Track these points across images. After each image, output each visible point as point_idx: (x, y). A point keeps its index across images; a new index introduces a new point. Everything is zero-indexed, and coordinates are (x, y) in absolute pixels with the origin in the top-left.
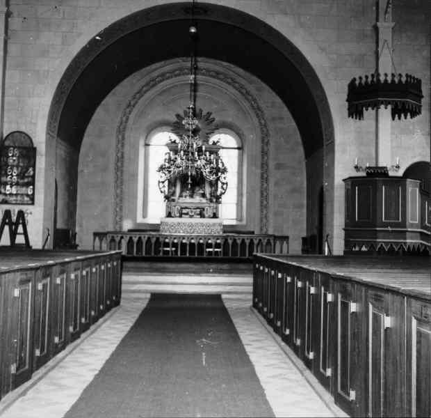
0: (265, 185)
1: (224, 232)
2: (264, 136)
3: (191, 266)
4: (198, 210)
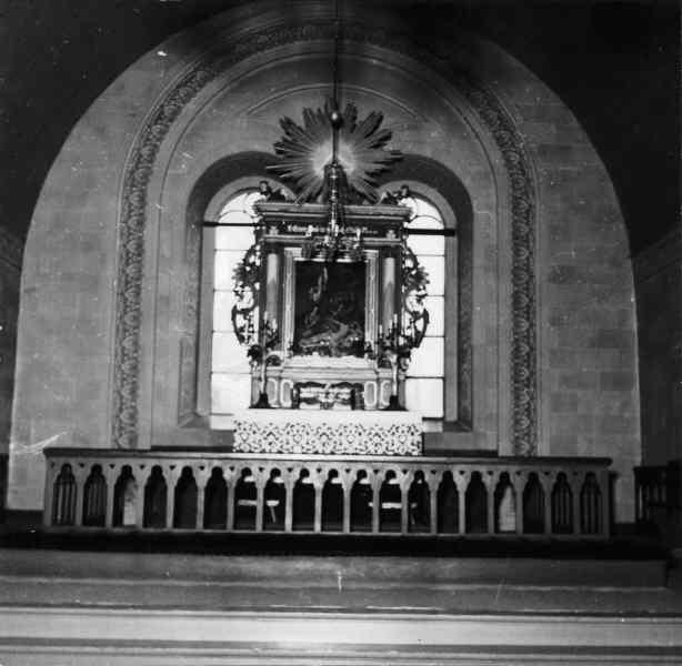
0: (525, 325)
1: (424, 453)
2: (518, 194)
3: (333, 569)
4: (347, 390)
